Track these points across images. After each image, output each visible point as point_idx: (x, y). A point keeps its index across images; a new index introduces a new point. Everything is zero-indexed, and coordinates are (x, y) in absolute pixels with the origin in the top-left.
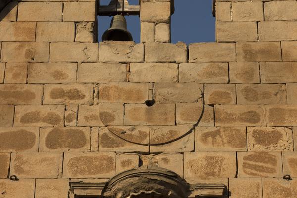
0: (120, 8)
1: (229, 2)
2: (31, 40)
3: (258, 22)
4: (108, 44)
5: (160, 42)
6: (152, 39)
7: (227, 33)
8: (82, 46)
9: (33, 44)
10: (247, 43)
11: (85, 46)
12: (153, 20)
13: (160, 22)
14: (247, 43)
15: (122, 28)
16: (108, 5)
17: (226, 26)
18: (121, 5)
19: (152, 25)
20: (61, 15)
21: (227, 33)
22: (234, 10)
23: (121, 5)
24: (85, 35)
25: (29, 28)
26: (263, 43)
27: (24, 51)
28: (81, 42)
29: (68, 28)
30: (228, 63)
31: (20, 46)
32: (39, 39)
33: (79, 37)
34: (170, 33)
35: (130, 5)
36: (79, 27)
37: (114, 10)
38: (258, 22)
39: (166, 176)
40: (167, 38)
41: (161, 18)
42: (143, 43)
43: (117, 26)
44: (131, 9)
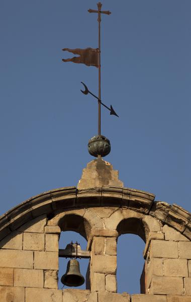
0: (74, 252)
1: (162, 258)
2: (10, 285)
3: (183, 278)
4: (70, 292)
5: (110, 292)
6: (103, 289)
7: (161, 286)
8: (49, 292)
9: (12, 288)
10: (176, 296)
11: (52, 293)
12: (104, 272)
13: (109, 274)
14: (176, 296)
15: (76, 273)
16: (64, 248)
17: (160, 280)
18: (76, 250)
19: (103, 275)
20: (32, 262)
21: (161, 286)
22: (165, 266)
23: (76, 250)
24: (51, 282)
25: (8, 274)
26: (188, 297)
27: (5, 294)
28: (48, 288)
29: (38, 275)
30: (44, 288)
31: (2, 290)
32: (17, 283)
33: (48, 284)
34: (117, 284)
35: (82, 250)
36: (47, 274)
37: (69, 254)
38: (183, 278)
39: (89, 190)
40: (114, 289)
41: (110, 270)
42: (97, 291)
43: (74, 271)
44: (83, 254)
